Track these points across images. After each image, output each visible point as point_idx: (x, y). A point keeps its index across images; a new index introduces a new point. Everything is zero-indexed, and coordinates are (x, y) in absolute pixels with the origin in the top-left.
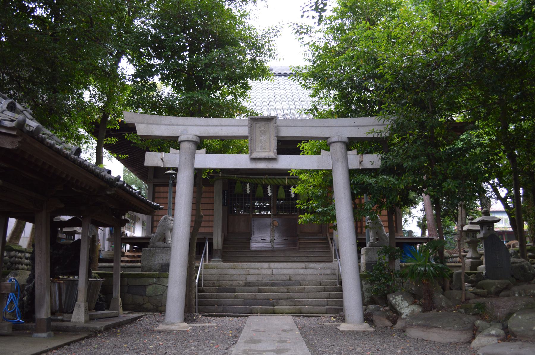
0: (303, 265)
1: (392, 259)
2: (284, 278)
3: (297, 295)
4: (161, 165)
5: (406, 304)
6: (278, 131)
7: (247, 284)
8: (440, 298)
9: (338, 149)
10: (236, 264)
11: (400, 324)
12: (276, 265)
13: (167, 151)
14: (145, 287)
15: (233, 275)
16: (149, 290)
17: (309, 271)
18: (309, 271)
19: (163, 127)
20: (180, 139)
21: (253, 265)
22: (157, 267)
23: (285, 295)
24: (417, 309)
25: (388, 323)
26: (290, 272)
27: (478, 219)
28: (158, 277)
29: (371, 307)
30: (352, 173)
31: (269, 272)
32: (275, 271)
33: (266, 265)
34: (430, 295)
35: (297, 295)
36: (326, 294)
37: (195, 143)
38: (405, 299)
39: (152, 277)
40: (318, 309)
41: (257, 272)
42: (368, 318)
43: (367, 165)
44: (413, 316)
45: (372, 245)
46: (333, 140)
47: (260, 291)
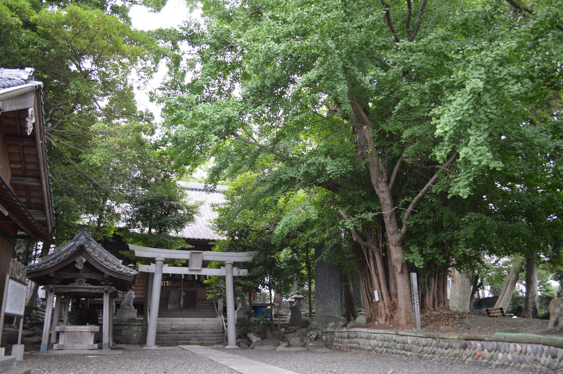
0: (202, 319)
1: (250, 317)
2: (192, 326)
3: (201, 335)
4: (147, 271)
5: (255, 337)
6: (202, 257)
7: (172, 330)
8: (269, 334)
9: (228, 267)
10: (165, 318)
11: (251, 346)
12: (187, 319)
13: (150, 264)
14: (121, 331)
15: (164, 325)
16: (124, 332)
17: (205, 323)
18: (205, 323)
19: (148, 253)
20: (156, 259)
21: (174, 319)
22: (126, 320)
23: (194, 335)
24: (259, 339)
25: (247, 346)
26: (195, 323)
27: (294, 296)
28: (129, 326)
29: (239, 340)
30: (234, 278)
31: (183, 323)
32: (187, 323)
33: (181, 319)
34: (265, 333)
35: (201, 335)
36: (216, 335)
37: (164, 261)
38: (254, 335)
39: (126, 325)
40: (212, 342)
41: (177, 323)
42: (237, 344)
43: (241, 274)
44: (257, 341)
45: (240, 309)
46: (227, 262)
47: (180, 333)
